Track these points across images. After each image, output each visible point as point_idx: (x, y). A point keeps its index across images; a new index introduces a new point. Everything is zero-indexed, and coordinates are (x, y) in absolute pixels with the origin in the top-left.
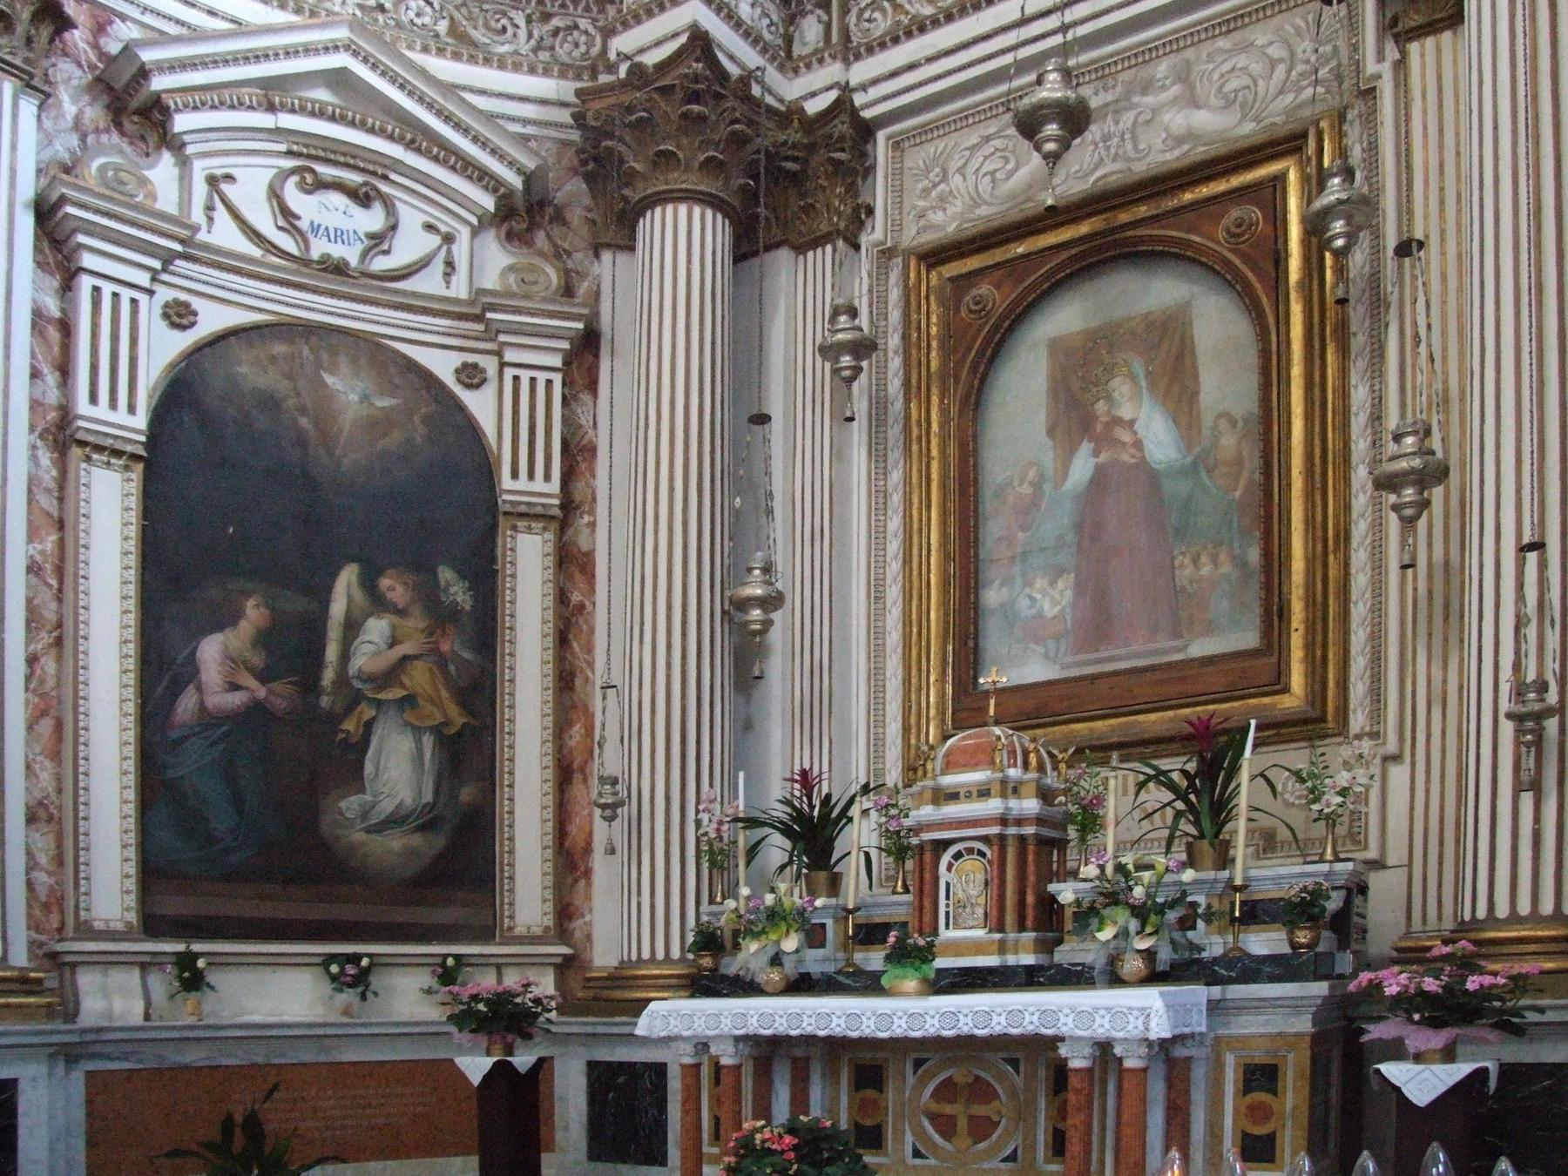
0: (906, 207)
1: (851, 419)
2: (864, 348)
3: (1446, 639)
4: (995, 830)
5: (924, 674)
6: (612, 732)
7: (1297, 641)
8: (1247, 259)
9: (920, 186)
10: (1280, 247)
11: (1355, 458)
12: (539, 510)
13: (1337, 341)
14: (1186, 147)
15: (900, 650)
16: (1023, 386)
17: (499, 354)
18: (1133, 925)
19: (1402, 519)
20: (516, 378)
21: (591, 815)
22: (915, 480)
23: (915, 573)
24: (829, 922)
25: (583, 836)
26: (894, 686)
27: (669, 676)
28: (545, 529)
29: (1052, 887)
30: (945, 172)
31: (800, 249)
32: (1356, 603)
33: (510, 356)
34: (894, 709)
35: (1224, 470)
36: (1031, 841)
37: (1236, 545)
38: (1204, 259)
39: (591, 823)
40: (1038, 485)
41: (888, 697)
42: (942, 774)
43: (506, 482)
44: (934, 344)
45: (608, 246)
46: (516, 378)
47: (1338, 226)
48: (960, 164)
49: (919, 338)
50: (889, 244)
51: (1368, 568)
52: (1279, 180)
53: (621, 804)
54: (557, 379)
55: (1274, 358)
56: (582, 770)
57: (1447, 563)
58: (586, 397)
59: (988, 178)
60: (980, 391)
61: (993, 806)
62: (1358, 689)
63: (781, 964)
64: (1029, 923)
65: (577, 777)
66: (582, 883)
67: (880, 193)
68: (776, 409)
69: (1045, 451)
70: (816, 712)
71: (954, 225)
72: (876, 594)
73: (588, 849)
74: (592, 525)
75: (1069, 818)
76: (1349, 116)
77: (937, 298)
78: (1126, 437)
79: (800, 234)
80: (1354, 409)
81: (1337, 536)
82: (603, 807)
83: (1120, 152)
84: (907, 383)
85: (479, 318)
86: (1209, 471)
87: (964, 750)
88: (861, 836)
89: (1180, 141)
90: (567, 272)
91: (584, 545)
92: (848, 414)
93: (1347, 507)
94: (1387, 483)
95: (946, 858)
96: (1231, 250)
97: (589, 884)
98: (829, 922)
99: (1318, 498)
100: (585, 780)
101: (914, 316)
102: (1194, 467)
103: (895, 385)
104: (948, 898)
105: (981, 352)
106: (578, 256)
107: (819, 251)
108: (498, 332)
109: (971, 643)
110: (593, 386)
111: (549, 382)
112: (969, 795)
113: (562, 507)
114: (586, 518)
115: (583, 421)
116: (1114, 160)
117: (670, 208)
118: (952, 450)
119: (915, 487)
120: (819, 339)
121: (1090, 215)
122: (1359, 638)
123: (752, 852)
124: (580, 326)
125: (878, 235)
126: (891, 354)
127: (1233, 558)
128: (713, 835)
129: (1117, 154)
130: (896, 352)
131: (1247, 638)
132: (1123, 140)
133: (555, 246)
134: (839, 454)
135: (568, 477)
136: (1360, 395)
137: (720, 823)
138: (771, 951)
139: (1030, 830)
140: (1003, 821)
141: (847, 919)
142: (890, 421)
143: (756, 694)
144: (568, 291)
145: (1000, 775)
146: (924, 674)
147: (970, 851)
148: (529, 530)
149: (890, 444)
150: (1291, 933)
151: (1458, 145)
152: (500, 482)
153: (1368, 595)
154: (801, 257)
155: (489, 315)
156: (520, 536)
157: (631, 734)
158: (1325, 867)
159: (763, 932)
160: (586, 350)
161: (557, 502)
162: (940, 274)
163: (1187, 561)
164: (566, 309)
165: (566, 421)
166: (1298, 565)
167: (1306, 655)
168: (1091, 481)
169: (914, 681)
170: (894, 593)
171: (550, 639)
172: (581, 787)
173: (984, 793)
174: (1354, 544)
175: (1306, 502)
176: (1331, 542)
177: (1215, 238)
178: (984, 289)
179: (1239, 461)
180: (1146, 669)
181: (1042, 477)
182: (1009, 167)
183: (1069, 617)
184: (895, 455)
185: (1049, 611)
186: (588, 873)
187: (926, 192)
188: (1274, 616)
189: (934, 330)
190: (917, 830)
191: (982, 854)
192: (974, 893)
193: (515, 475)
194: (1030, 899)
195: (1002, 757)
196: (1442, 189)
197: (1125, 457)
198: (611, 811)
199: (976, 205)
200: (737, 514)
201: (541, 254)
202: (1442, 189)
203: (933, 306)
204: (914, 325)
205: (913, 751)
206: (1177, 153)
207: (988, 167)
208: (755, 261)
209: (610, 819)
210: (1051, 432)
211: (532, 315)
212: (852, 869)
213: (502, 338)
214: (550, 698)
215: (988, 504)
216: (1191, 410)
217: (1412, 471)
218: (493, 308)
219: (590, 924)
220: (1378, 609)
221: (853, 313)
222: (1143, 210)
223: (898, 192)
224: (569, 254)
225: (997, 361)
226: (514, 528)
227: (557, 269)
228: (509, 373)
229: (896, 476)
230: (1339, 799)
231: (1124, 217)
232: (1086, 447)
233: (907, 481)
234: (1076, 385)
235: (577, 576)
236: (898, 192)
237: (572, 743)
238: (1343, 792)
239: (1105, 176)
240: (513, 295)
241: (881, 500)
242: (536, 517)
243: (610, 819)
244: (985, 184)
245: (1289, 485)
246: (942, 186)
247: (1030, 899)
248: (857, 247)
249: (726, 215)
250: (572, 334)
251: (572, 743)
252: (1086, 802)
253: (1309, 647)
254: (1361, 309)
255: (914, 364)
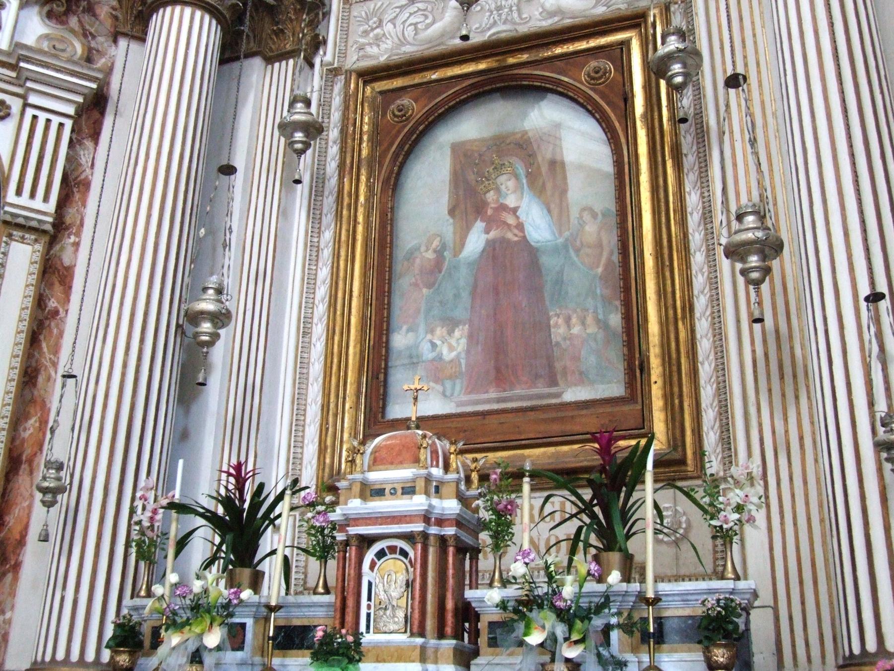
0: (350, 43)
1: (298, 182)
2: (313, 130)
3: (783, 395)
4: (418, 527)
5: (341, 400)
6: (65, 421)
7: (656, 391)
8: (603, 96)
9: (361, 29)
10: (627, 88)
11: (693, 247)
12: (34, 224)
13: (673, 158)
14: (556, 19)
15: (321, 380)
16: (430, 178)
17: (24, 97)
18: (560, 630)
19: (749, 282)
20: (35, 117)
21: (32, 496)
22: (343, 238)
23: (338, 313)
24: (249, 622)
25: (19, 528)
26: (313, 411)
27: (123, 374)
28: (36, 240)
29: (469, 594)
30: (381, 21)
31: (269, 60)
32: (702, 364)
33: (33, 99)
34: (312, 432)
35: (589, 251)
36: (451, 542)
37: (600, 311)
38: (570, 94)
39: (30, 507)
40: (439, 253)
41: (308, 421)
42: (370, 470)
43: (11, 196)
44: (365, 138)
45: (125, 35)
46: (35, 117)
47: (677, 68)
48: (392, 17)
49: (354, 131)
50: (336, 65)
51: (710, 335)
52: (625, 45)
53: (60, 490)
54: (69, 124)
55: (626, 167)
56: (30, 462)
57: (777, 331)
58: (89, 144)
59: (412, 27)
60: (399, 174)
61: (418, 502)
62: (711, 439)
63: (201, 662)
64: (449, 630)
65: (25, 467)
66: (9, 577)
67: (332, 30)
68: (239, 162)
69: (448, 228)
70: (246, 423)
71: (385, 57)
72: (305, 332)
73: (21, 542)
74: (77, 245)
75: (483, 525)
76: (672, 9)
77: (369, 106)
78: (511, 220)
79: (271, 50)
80: (689, 210)
81: (683, 308)
82: (44, 491)
83: (509, 18)
84: (341, 166)
85: (14, 67)
86: (577, 251)
87: (389, 448)
88: (278, 540)
89: (552, 14)
90: (90, 50)
91: (67, 261)
92: (297, 177)
93: (690, 284)
94: (735, 252)
95: (370, 556)
96: (591, 89)
97: (16, 579)
98: (249, 622)
99: (668, 274)
100: (31, 472)
101: (352, 116)
102: (565, 246)
103: (332, 166)
104: (369, 599)
105: (401, 146)
106: (100, 39)
107: (284, 63)
108: (27, 79)
109: (382, 377)
110: (95, 136)
111: (61, 125)
112: (393, 492)
113: (54, 225)
114: (73, 239)
115: (83, 161)
116: (504, 23)
117: (178, 9)
118: (375, 219)
119: (343, 246)
120: (278, 120)
121: (485, 57)
122: (707, 393)
123: (182, 543)
124: (94, 86)
125: (328, 58)
126: (330, 143)
127: (598, 321)
128: (146, 524)
129: (506, 19)
130: (335, 142)
131: (617, 389)
132: (511, 11)
133: (84, 29)
134: (284, 213)
135: (64, 201)
136: (693, 199)
137: (155, 512)
138: (192, 647)
139: (450, 531)
140: (426, 518)
141: (267, 619)
142: (326, 193)
143: (194, 408)
144: (89, 60)
145: (423, 472)
146: (341, 400)
147: (392, 549)
148: (22, 240)
149: (325, 211)
150: (707, 652)
151: (753, 29)
152: (5, 197)
153: (712, 357)
154: (270, 67)
155: (22, 64)
156: (14, 243)
157: (83, 426)
158: (728, 585)
159: (187, 623)
160: (94, 108)
161: (50, 220)
162: (373, 89)
163: (560, 321)
164: (85, 71)
165: (69, 159)
166: (654, 327)
167: (666, 404)
168: (483, 251)
169: (332, 406)
170: (319, 330)
171: (23, 335)
172: (28, 479)
173: (409, 490)
174: (697, 314)
175: (658, 277)
176: (679, 311)
177: (580, 79)
178: (406, 101)
179: (600, 245)
180: (532, 409)
181: (444, 247)
182: (428, 21)
183: (463, 362)
184: (328, 219)
185: (448, 355)
186: (17, 567)
187: (366, 33)
188: (636, 369)
189: (366, 128)
190: (349, 521)
191: (404, 553)
192: (395, 594)
193: (19, 192)
194: (450, 605)
195: (425, 455)
196: (745, 57)
197: (509, 235)
198: (51, 495)
199: (402, 44)
200: (199, 241)
201: (72, 31)
202: (745, 57)
203: (366, 110)
204: (351, 121)
205: (327, 470)
206: (550, 22)
207: (412, 20)
208: (236, 65)
209: (49, 505)
210: (452, 212)
211: (58, 71)
212: (272, 569)
213: (29, 84)
214: (13, 389)
215: (399, 266)
216: (561, 201)
217: (757, 241)
218: (28, 60)
219: (9, 622)
220: (721, 368)
221: (308, 103)
222: (525, 57)
223: (345, 31)
224: (94, 37)
225: (412, 156)
226: (10, 236)
227: (83, 44)
228: (30, 112)
229: (328, 235)
230: (736, 516)
231: (511, 60)
232: (479, 225)
233: (337, 241)
234: (471, 177)
235: (57, 284)
236: (345, 31)
237: (26, 435)
238: (739, 508)
239: (498, 33)
240: (45, 53)
241: (314, 254)
242: (32, 229)
243: (49, 505)
244: (410, 32)
245: (643, 264)
246: (378, 31)
247: (450, 605)
248: (312, 66)
249: (219, 22)
250: (86, 91)
251: (26, 435)
252: (501, 506)
253: (668, 397)
254: (689, 138)
255: (349, 150)
